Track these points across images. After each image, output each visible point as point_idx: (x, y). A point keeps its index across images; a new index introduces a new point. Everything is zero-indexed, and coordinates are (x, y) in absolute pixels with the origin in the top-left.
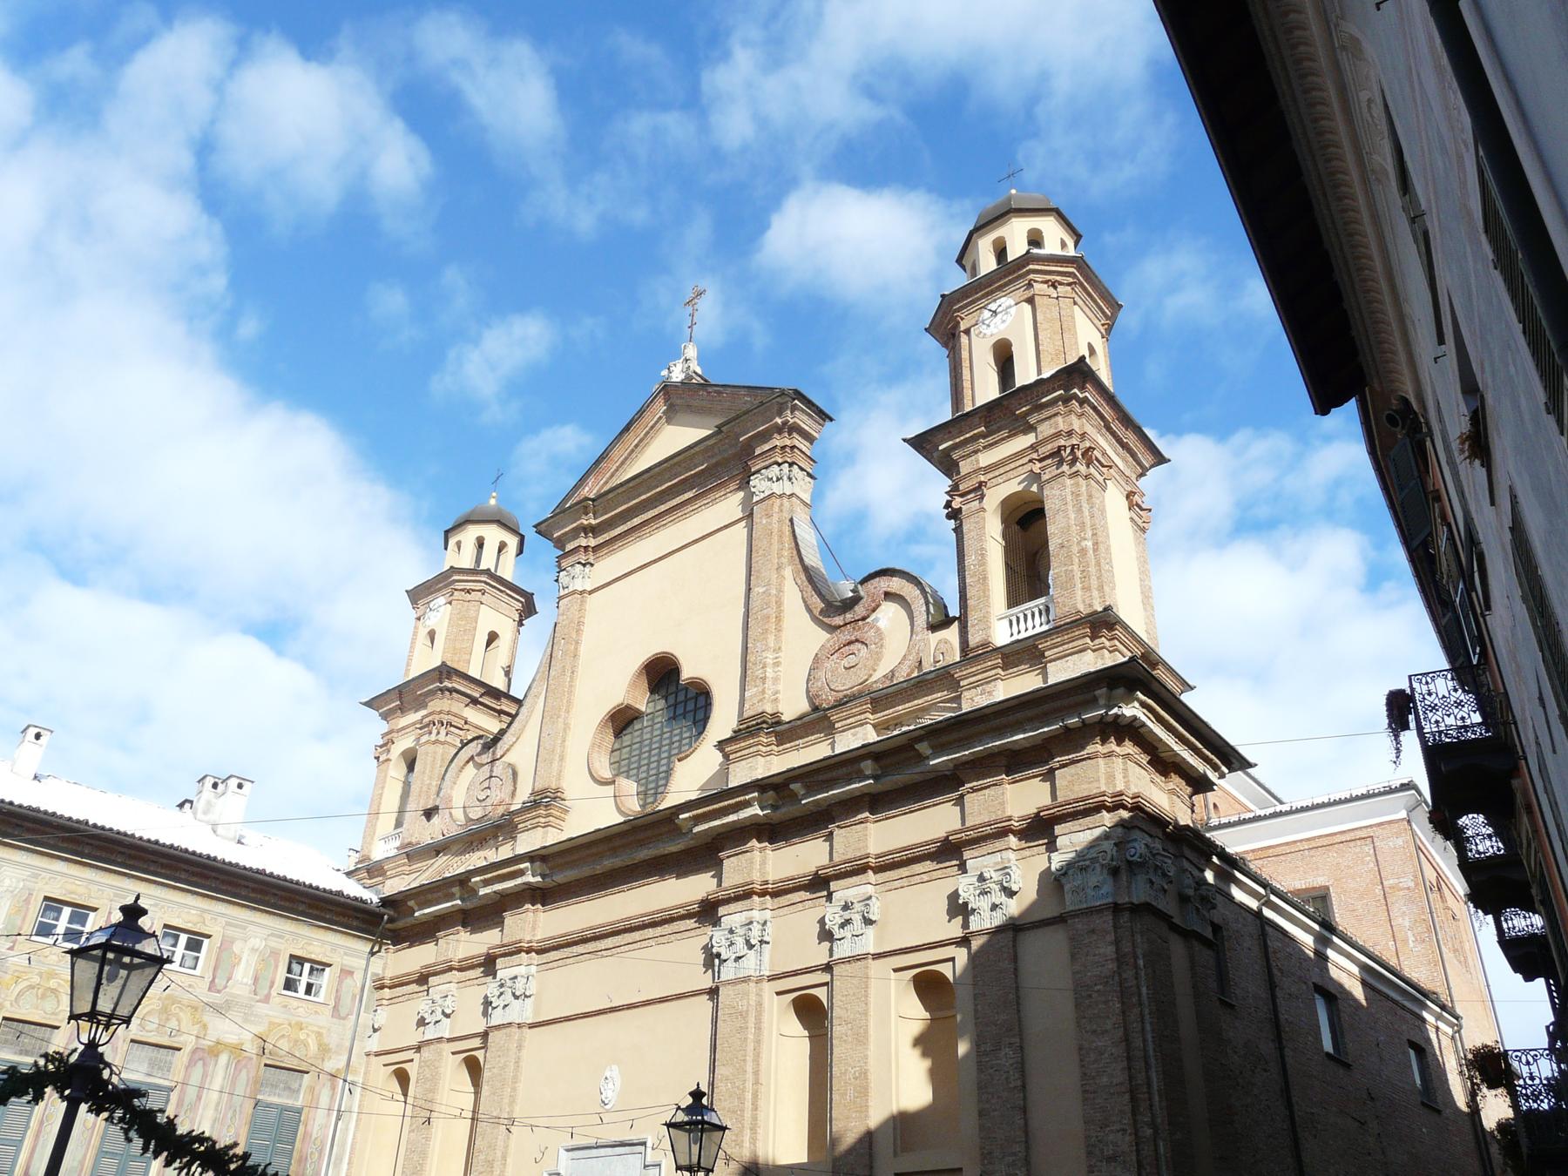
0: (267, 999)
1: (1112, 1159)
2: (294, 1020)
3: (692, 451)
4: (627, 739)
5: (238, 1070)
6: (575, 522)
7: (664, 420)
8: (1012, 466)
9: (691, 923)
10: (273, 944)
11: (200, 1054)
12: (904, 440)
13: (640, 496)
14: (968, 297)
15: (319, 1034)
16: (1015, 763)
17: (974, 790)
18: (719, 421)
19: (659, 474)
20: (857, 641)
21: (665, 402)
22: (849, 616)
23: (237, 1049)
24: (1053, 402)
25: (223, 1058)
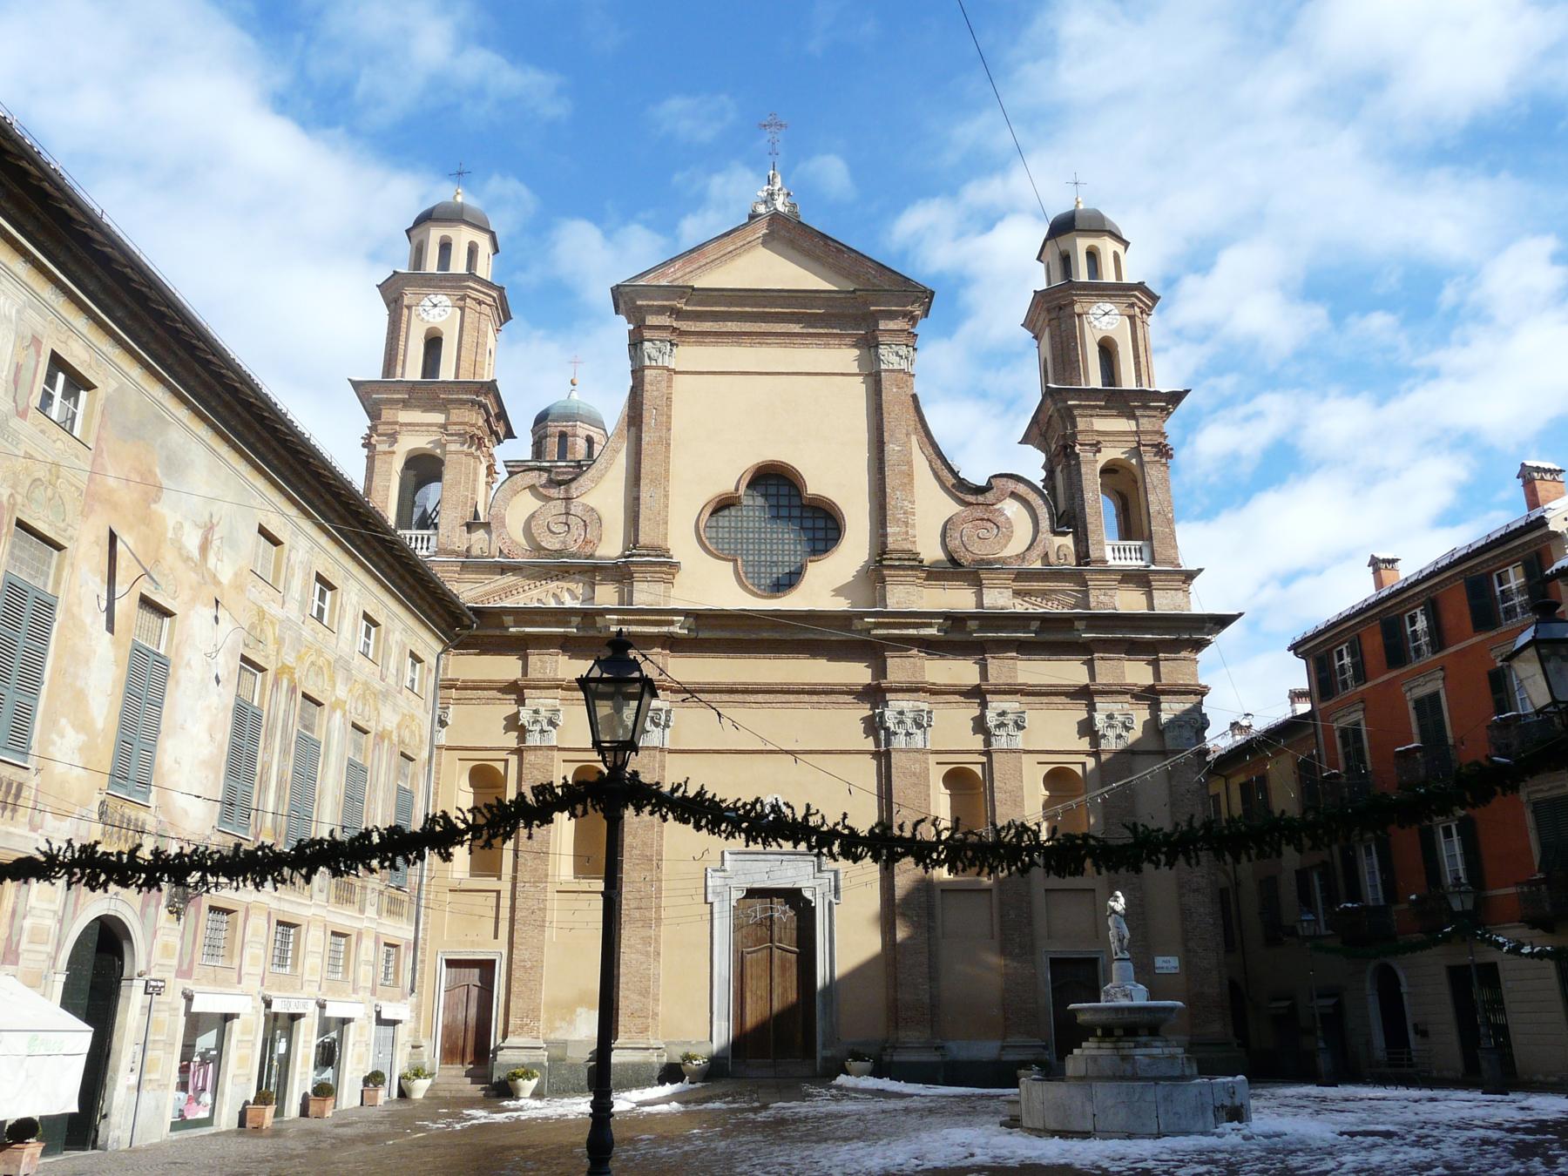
1: (1196, 891)
3: (817, 295)
4: (723, 522)
6: (666, 300)
7: (760, 240)
9: (849, 698)
13: (745, 306)
14: (1085, 290)
16: (1133, 649)
17: (1102, 659)
18: (857, 287)
20: (988, 520)
21: (768, 226)
22: (981, 499)
24: (1156, 408)
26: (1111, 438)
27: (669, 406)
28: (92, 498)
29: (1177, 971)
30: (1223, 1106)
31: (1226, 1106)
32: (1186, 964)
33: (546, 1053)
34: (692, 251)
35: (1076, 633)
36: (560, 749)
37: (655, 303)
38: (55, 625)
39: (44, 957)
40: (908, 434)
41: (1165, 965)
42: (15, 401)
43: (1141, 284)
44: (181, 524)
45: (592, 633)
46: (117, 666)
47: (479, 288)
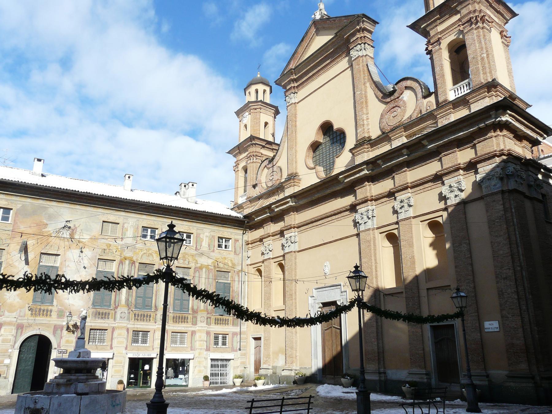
1: (505, 278)
2: (223, 257)
3: (327, 45)
4: (317, 153)
7: (315, 35)
10: (212, 234)
16: (460, 143)
17: (445, 155)
18: (335, 32)
20: (396, 106)
21: (315, 28)
22: (392, 98)
26: (447, 32)
27: (296, 117)
29: (498, 330)
30: (29, 408)
31: (31, 408)
32: (503, 325)
33: (272, 371)
34: (293, 55)
36: (272, 258)
37: (286, 81)
39: (10, 346)
40: (364, 84)
41: (490, 326)
47: (254, 104)
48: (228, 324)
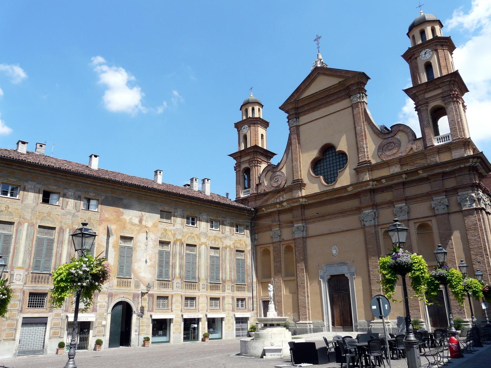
0: (233, 235)
5: (231, 251)
8: (435, 98)
11: (223, 249)
12: (403, 90)
15: (245, 242)
19: (319, 93)
23: (230, 247)
25: (228, 249)
28: (101, 221)
35: (421, 175)
38: (95, 248)
42: (76, 209)
43: (316, 68)
44: (132, 218)
45: (283, 208)
46: (115, 252)
48: (245, 291)
